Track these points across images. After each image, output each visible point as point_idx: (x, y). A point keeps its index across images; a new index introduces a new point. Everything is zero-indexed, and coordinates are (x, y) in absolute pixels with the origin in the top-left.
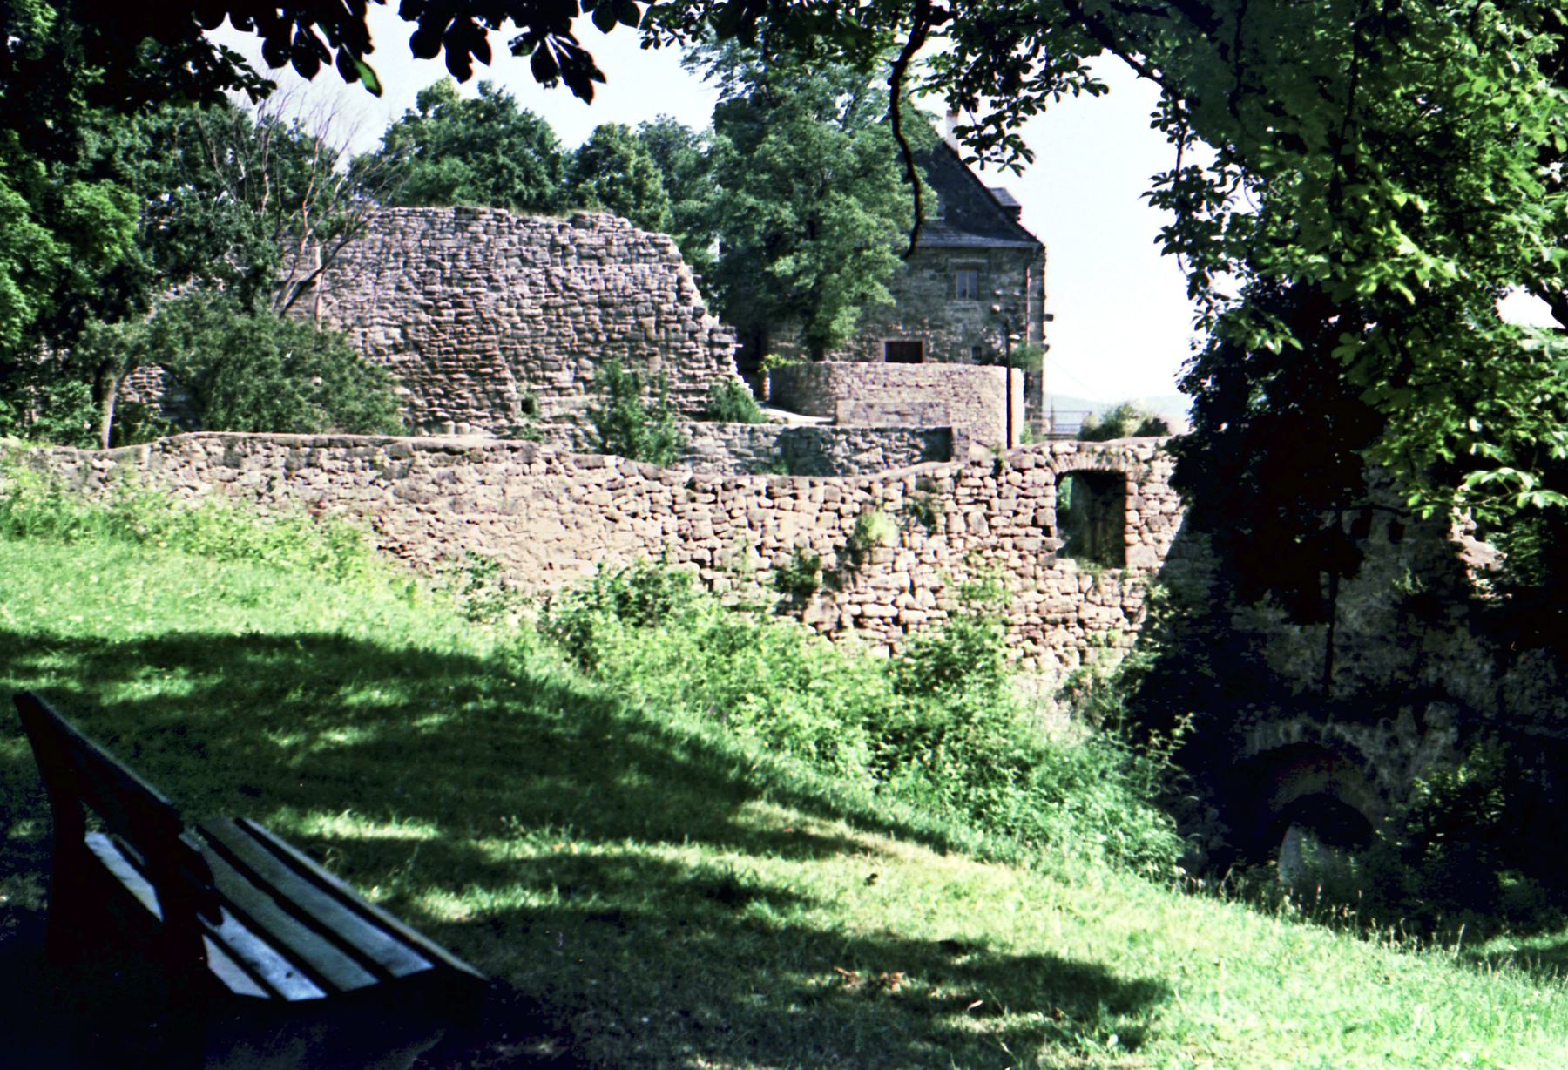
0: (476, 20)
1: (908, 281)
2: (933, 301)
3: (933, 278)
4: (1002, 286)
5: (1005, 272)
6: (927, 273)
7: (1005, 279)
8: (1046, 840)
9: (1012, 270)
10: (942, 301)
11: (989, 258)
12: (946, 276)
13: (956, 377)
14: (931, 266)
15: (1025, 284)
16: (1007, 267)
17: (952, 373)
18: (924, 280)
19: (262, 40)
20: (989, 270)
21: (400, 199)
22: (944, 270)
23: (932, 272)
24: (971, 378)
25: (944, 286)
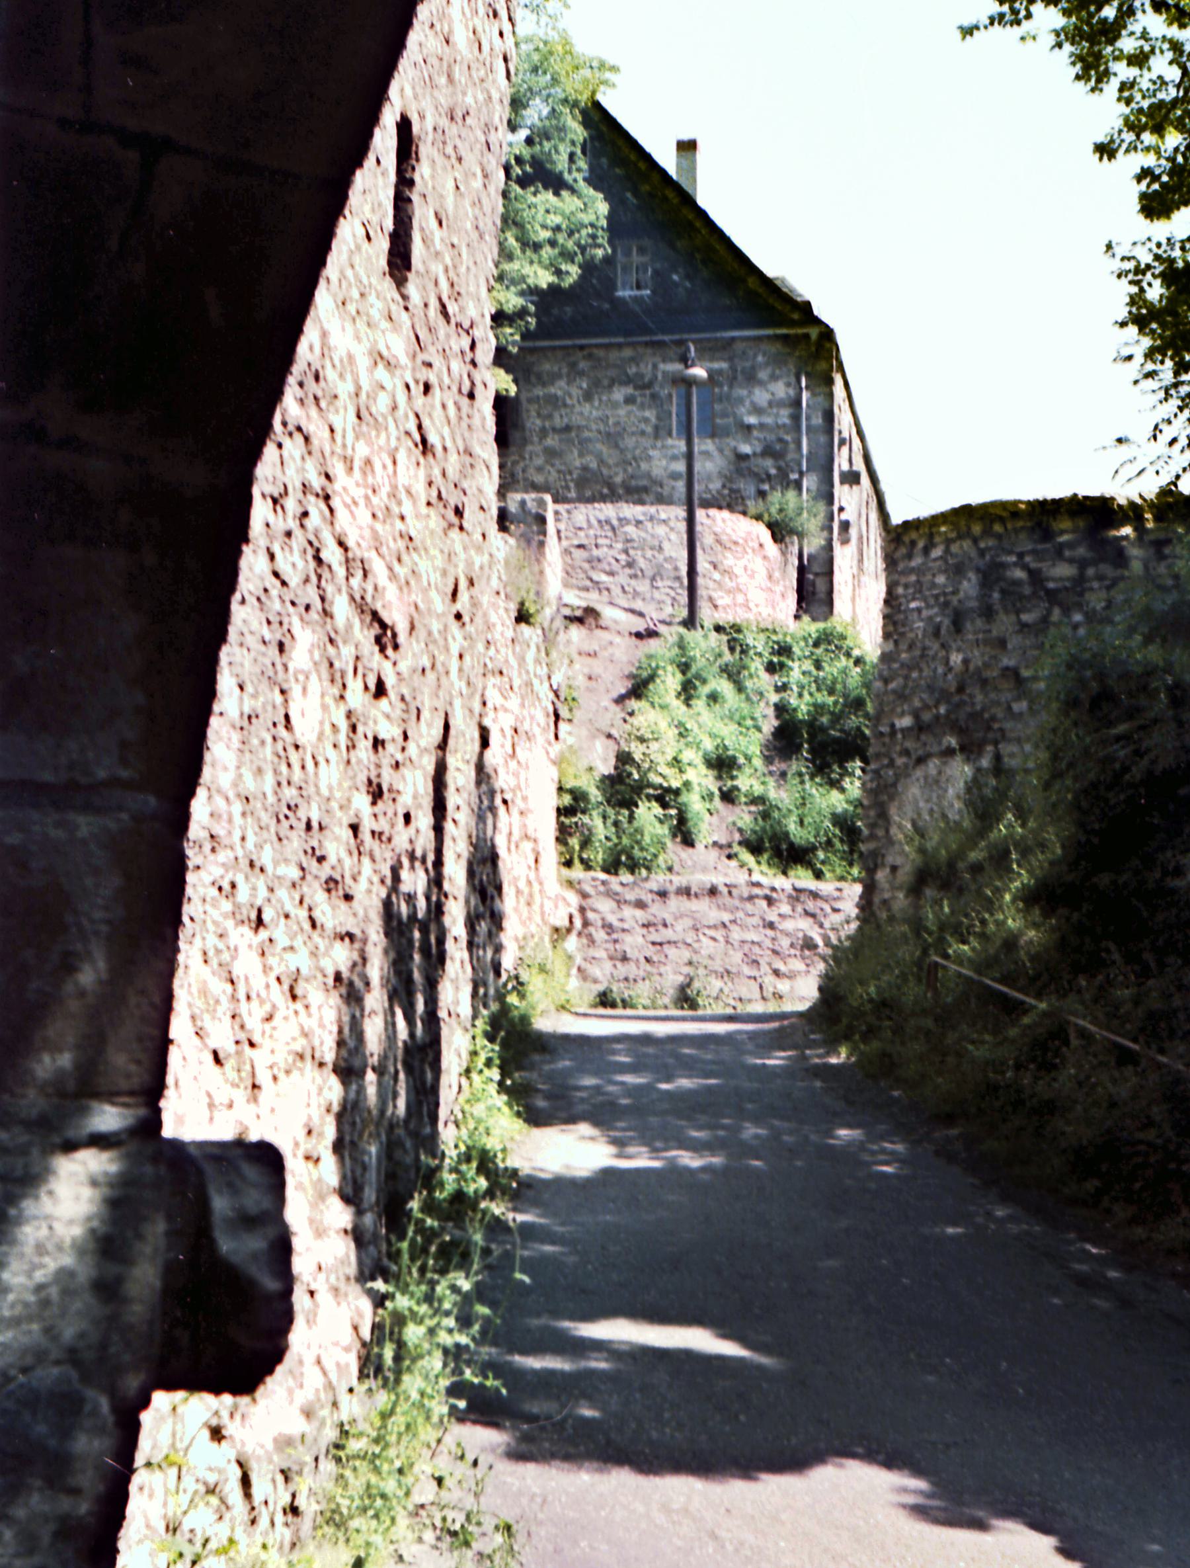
0: (526, 1279)
1: (586, 408)
2: (630, 442)
3: (629, 400)
4: (757, 410)
5: (761, 383)
6: (619, 394)
7: (761, 396)
8: (790, 897)
9: (774, 378)
10: (645, 442)
11: (731, 359)
12: (654, 396)
13: (630, 529)
14: (628, 381)
15: (797, 403)
16: (763, 375)
17: (623, 521)
18: (615, 405)
19: (545, 286)
20: (732, 381)
21: (398, 1154)
22: (649, 385)
23: (629, 390)
24: (661, 530)
25: (650, 414)
